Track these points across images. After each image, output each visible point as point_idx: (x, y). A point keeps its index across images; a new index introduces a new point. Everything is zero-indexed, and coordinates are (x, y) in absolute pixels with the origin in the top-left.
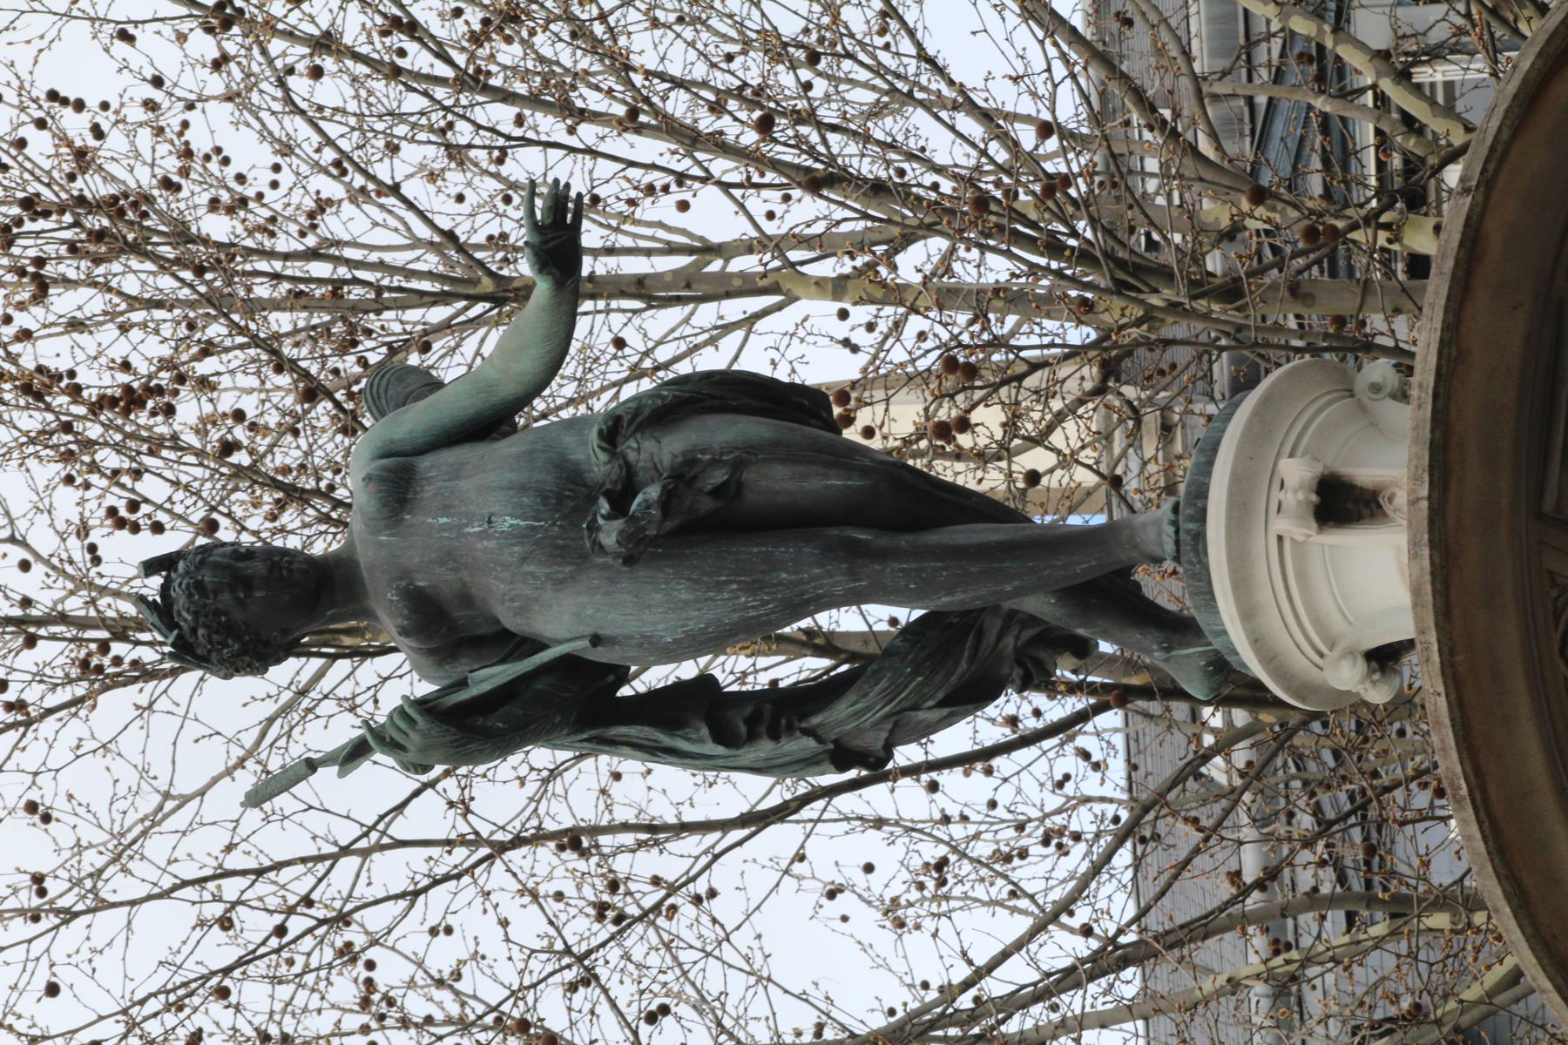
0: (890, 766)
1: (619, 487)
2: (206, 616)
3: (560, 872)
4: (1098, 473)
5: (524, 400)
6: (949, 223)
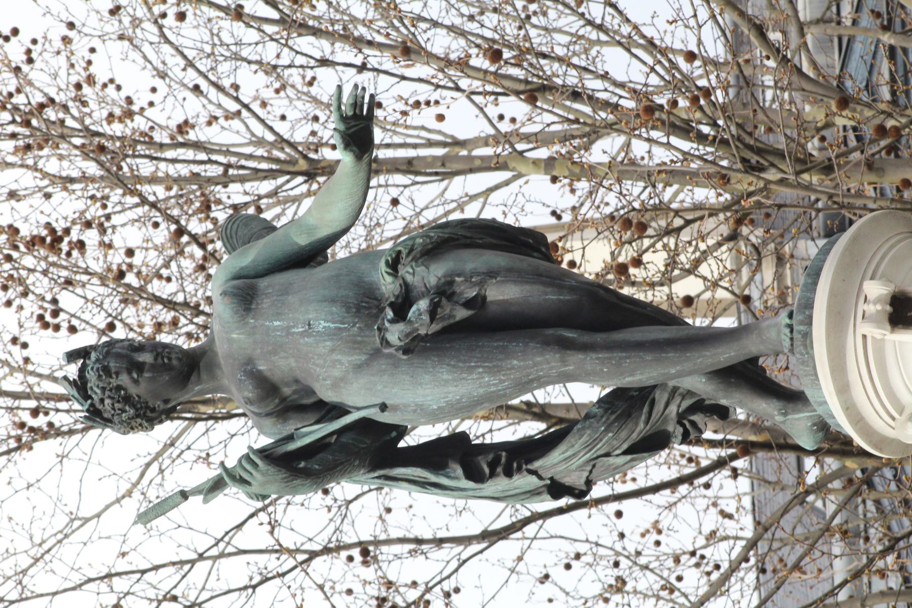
0: (588, 498)
1: (400, 300)
2: (111, 390)
3: (349, 576)
4: (733, 293)
5: (332, 239)
6: (626, 124)
